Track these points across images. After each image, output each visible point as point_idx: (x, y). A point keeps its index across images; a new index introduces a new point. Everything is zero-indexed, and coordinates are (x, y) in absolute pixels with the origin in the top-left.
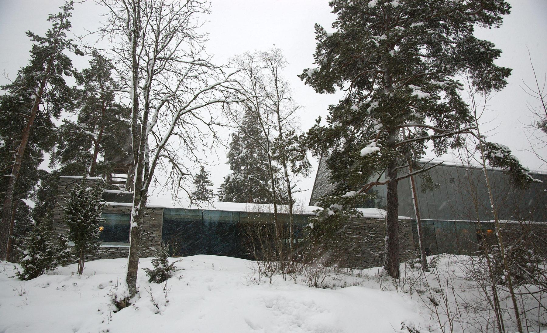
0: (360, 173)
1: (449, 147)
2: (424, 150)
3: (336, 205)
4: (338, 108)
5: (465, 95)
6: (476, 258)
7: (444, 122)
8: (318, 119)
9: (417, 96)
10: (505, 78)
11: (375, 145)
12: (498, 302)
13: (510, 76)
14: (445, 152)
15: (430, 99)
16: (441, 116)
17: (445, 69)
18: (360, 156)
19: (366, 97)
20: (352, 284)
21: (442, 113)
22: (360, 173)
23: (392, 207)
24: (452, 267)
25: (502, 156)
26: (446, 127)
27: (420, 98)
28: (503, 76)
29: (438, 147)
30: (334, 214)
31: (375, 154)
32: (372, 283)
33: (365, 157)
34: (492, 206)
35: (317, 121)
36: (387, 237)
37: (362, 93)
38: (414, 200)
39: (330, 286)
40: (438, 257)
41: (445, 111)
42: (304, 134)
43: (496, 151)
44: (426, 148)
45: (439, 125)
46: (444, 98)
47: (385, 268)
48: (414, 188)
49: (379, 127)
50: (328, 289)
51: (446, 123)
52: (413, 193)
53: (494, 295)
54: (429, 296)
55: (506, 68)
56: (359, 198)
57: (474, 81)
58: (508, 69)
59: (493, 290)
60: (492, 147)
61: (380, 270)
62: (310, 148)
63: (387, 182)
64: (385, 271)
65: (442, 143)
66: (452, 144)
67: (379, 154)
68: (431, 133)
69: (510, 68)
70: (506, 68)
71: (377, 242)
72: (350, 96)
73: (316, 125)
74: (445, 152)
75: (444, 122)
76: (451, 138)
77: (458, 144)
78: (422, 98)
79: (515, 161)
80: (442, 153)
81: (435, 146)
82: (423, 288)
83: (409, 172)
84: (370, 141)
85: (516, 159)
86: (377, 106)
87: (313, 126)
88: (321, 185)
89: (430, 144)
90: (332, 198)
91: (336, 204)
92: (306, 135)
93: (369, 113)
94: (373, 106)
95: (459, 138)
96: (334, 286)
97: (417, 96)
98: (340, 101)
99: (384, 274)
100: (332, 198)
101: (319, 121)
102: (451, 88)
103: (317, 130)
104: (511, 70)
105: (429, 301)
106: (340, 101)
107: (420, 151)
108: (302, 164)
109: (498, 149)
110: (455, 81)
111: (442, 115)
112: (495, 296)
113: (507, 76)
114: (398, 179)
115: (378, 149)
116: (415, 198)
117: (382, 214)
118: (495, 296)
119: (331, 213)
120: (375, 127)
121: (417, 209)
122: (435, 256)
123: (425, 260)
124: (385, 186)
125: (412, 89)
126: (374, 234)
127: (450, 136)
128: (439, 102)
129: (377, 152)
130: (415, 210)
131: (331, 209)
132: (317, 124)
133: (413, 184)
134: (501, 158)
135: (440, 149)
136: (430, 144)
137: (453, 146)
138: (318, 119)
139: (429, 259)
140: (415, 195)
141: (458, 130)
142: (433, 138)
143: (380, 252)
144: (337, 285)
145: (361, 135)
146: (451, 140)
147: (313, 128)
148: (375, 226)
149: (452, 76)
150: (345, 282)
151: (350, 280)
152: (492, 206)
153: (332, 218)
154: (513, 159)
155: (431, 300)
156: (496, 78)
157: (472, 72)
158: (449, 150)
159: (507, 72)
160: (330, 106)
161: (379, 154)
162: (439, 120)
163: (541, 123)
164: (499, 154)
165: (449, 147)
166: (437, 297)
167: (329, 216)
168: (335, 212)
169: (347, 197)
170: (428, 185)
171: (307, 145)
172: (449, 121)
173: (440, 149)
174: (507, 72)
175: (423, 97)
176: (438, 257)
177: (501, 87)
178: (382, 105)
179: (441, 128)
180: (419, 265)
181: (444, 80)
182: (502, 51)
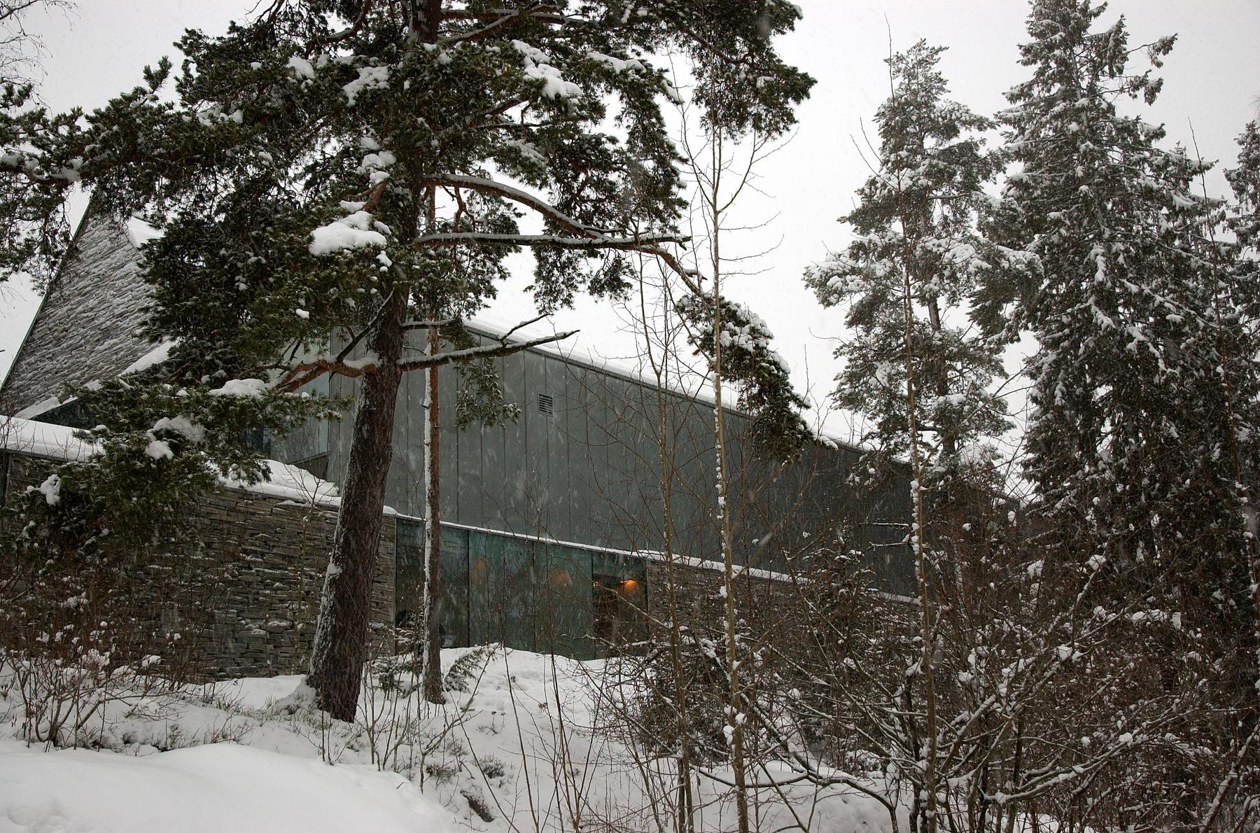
0: (304, 314)
1: (581, 287)
2: (496, 282)
3: (180, 424)
4: (221, 49)
5: (683, 123)
6: (596, 665)
7: (584, 200)
8: (155, 68)
9: (541, 84)
10: (791, 104)
11: (365, 225)
12: (690, 810)
13: (805, 102)
14: (567, 302)
15: (582, 107)
16: (575, 178)
17: (634, 19)
18: (307, 252)
19: (335, 40)
20: (210, 738)
21: (584, 169)
22: (304, 314)
23: (369, 462)
24: (528, 694)
25: (750, 347)
26: (586, 217)
27: (552, 96)
28: (786, 97)
29: (547, 279)
30: (170, 454)
31: (367, 255)
32: (278, 730)
33: (328, 260)
34: (721, 501)
35: (149, 75)
36: (332, 569)
37: (323, 21)
38: (427, 449)
39: (112, 740)
40: (479, 653)
41: (597, 166)
42: (77, 113)
43: (737, 329)
44: (503, 277)
45: (566, 206)
46: (619, 118)
47: (309, 682)
48: (434, 408)
49: (381, 164)
50: (104, 754)
51: (589, 206)
52: (428, 425)
53: (682, 789)
54: (466, 787)
55: (800, 71)
56: (281, 408)
57: (701, 89)
58: (805, 76)
59: (681, 770)
60: (729, 315)
61: (289, 686)
62: (86, 176)
63: (370, 372)
64: (311, 692)
65: (562, 269)
66: (596, 281)
67: (383, 257)
68: (532, 224)
69: (811, 75)
70: (800, 71)
71: (266, 586)
72: (273, 18)
73: (139, 92)
74: (567, 302)
75: (584, 200)
76: (591, 260)
77: (611, 283)
78: (558, 96)
79: (779, 369)
80: (558, 304)
81: (538, 274)
82: (450, 761)
83: (428, 350)
84: (345, 204)
85: (783, 365)
86: (383, 85)
87: (129, 91)
88: (58, 341)
89: (521, 264)
90: (173, 393)
91: (179, 418)
92: (84, 125)
93: (352, 102)
94: (369, 80)
95: (618, 261)
96: (127, 742)
97: (541, 84)
98: (234, 28)
99: (305, 705)
100: (173, 393)
101: (156, 79)
102: (642, 91)
103: (143, 110)
104: (812, 82)
105: (466, 807)
106: (234, 28)
107: (482, 281)
108: (37, 236)
109: (740, 323)
110: (655, 68)
111: (582, 177)
112: (685, 789)
113: (798, 100)
114: (404, 367)
115: (380, 240)
116: (434, 445)
117: (303, 487)
118: (685, 789)
119: (159, 449)
120: (369, 159)
121: (434, 482)
122: (469, 650)
123: (435, 661)
124: (359, 382)
125: (522, 56)
126: (263, 555)
127: (592, 251)
128: (588, 128)
129: (377, 249)
130: (428, 486)
131: (159, 436)
132: (146, 86)
133: (434, 395)
134: (746, 352)
135: (552, 288)
136: (521, 264)
137: (597, 288)
138: (155, 68)
139: (449, 657)
140: (434, 434)
141: (618, 237)
142: (538, 245)
143: (274, 623)
144: (141, 738)
145: (309, 177)
146: (591, 266)
147: (128, 99)
148: (266, 526)
149: (649, 49)
150: (174, 728)
151: (195, 719)
152: (721, 501)
153: (160, 469)
154: (775, 363)
155: (474, 804)
156: (770, 98)
157: (701, 57)
158: (582, 296)
159: (799, 86)
160: (192, 33)
161: (383, 257)
162: (568, 188)
163: (817, 275)
164: (744, 340)
165: (581, 287)
166: (487, 793)
167: (149, 460)
168: (173, 447)
169: (232, 400)
170: (483, 408)
171: (78, 161)
172: (600, 200)
173: (552, 288)
174: (799, 86)
175: (563, 93)
176: (479, 653)
177: (777, 129)
178: (407, 85)
179: (569, 215)
180: (406, 678)
181: (623, 57)
182: (803, 13)
